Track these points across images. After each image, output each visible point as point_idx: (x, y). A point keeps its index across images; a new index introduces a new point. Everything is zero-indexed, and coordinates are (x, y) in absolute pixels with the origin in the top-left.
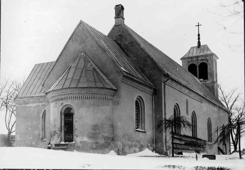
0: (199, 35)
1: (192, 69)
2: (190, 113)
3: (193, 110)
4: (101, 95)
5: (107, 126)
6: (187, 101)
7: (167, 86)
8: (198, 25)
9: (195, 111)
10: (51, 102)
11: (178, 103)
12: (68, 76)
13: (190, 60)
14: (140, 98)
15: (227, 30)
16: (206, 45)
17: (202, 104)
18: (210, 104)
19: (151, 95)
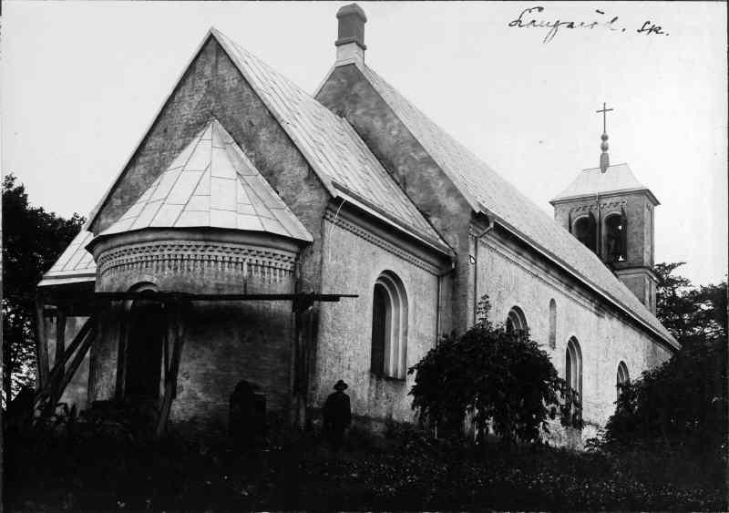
0: (604, 138)
1: (586, 230)
2: (562, 345)
3: (574, 334)
4: (228, 252)
5: (574, 433)
6: (553, 302)
7: (481, 249)
8: (605, 110)
9: (577, 337)
10: (409, 373)
11: (521, 307)
12: (155, 196)
13: (581, 204)
14: (386, 276)
15: (624, 27)
16: (657, 203)
17: (602, 320)
18: (377, 139)
19: (434, 274)
